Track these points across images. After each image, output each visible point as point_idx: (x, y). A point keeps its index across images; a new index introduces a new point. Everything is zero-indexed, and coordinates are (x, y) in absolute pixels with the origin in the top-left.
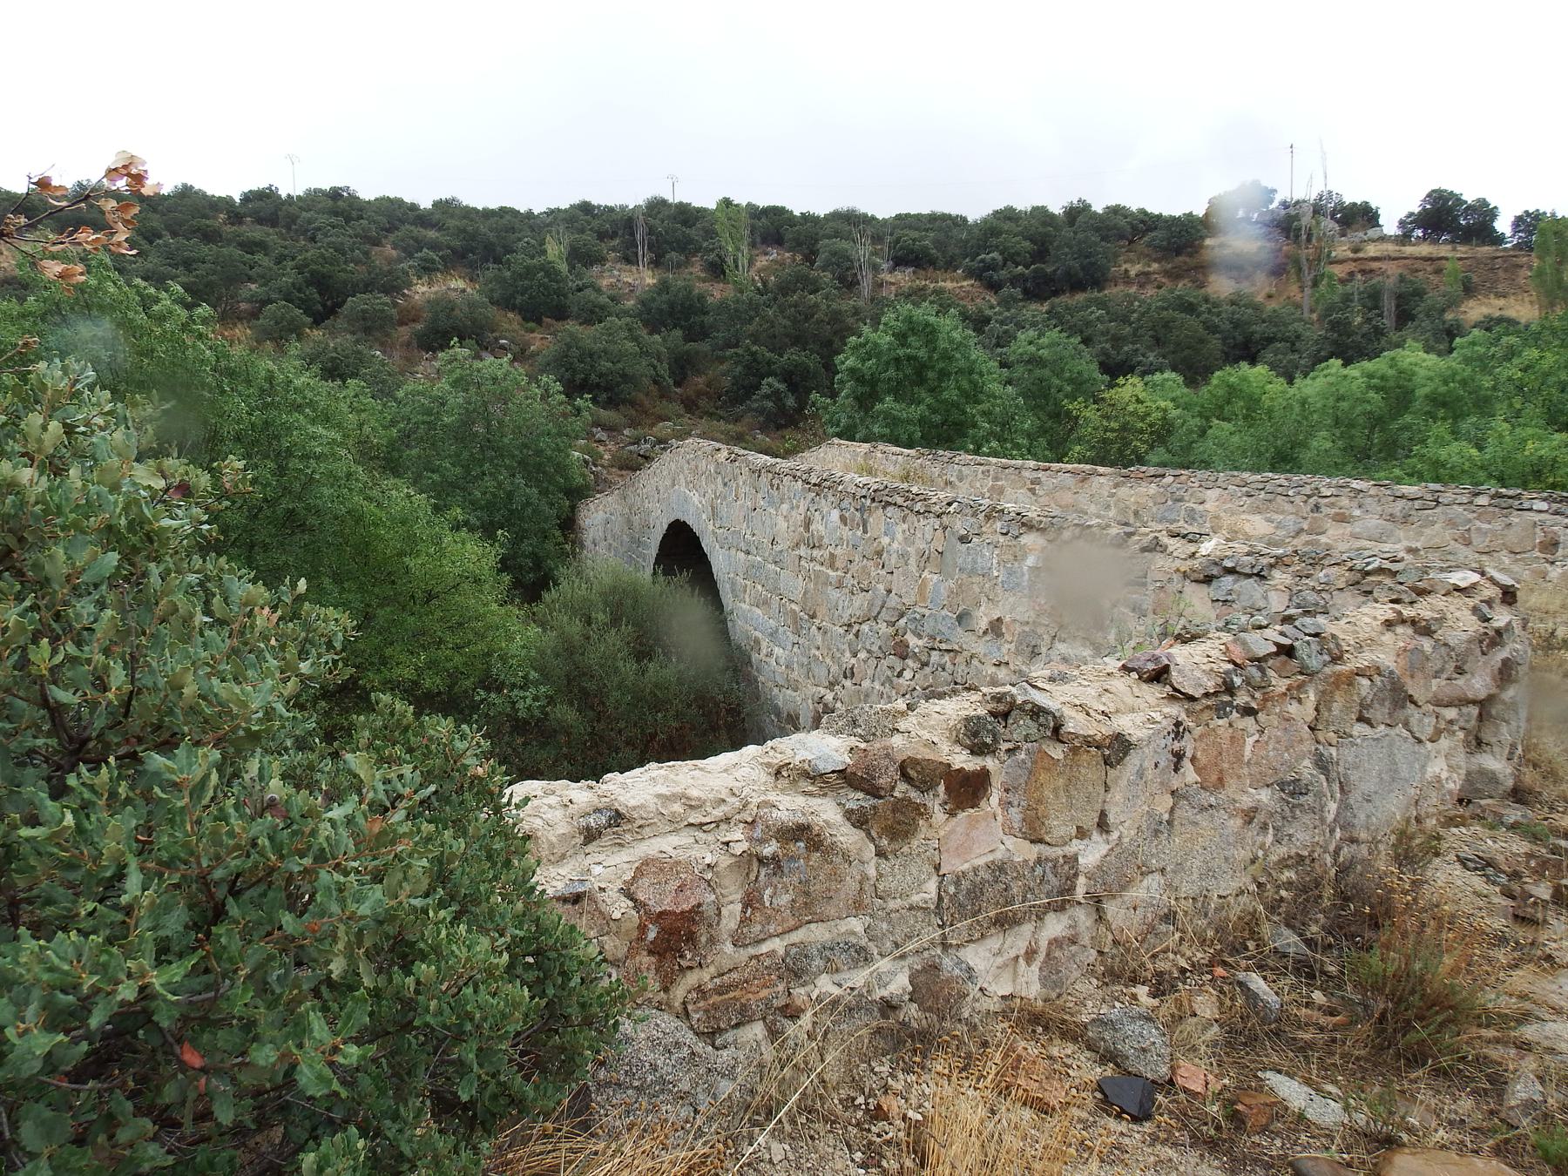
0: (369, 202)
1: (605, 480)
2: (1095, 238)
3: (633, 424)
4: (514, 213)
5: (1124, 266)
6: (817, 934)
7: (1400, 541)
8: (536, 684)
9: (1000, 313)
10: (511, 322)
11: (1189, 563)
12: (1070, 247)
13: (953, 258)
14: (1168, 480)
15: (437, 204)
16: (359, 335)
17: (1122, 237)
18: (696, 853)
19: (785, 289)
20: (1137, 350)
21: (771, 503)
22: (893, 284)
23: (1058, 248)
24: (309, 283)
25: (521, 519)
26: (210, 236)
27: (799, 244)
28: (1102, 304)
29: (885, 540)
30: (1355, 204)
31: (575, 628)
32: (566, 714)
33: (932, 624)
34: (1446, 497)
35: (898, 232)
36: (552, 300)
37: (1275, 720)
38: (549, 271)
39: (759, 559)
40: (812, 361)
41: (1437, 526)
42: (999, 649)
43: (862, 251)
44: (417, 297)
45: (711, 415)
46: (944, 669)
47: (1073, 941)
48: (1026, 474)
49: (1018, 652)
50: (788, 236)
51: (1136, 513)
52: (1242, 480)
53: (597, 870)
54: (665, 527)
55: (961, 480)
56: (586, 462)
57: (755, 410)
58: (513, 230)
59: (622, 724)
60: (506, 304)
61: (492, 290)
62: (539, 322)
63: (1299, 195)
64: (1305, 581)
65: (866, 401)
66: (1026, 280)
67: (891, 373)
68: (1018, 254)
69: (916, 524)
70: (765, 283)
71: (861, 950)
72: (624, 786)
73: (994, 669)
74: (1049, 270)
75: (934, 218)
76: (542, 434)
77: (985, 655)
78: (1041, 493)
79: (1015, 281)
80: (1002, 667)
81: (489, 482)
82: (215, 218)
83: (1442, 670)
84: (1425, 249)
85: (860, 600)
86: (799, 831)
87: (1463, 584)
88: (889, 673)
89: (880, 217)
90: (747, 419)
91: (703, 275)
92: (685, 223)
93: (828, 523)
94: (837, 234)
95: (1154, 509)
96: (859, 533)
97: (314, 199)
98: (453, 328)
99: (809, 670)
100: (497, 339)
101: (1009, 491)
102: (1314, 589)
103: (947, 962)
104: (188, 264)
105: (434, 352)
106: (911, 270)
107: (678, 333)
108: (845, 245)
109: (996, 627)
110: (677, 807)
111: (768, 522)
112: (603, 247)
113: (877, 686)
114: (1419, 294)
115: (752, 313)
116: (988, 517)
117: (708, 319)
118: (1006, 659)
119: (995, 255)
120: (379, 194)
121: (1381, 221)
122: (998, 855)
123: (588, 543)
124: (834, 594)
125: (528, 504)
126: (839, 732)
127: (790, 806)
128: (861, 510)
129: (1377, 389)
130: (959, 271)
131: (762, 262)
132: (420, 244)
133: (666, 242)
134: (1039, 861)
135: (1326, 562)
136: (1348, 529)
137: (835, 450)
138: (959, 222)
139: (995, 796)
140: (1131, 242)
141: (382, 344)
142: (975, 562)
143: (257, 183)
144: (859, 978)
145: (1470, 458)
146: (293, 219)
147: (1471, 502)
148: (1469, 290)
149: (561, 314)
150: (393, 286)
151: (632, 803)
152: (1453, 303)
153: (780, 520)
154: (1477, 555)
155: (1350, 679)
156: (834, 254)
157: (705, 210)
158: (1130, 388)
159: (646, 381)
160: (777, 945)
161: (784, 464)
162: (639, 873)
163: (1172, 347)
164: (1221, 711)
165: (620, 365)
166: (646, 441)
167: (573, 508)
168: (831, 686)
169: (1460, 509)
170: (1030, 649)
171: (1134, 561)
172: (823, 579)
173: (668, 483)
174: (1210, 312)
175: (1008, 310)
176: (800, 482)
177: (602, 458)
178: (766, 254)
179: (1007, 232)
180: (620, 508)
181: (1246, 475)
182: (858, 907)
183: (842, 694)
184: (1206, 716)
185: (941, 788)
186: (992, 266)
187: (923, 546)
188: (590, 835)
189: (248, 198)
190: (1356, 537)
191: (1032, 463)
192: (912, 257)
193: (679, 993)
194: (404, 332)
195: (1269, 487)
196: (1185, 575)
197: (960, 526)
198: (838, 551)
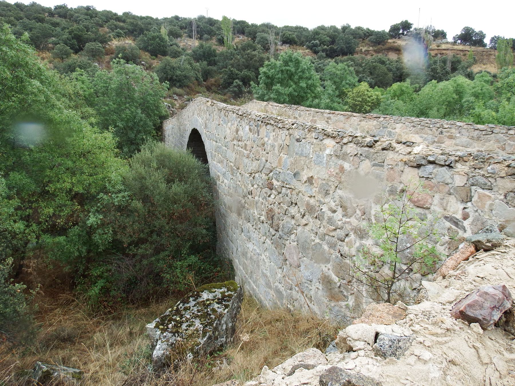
0: (100, 12)
2: (351, 37)
3: (188, 94)
4: (152, 18)
7: (475, 147)
10: (146, 56)
11: (407, 157)
12: (343, 40)
13: (303, 42)
14: (382, 119)
15: (125, 14)
16: (91, 58)
17: (360, 38)
19: (244, 49)
21: (225, 122)
23: (339, 40)
24: (73, 38)
25: (138, 126)
26: (41, 20)
27: (250, 34)
28: (352, 60)
29: (266, 139)
30: (439, 30)
31: (142, 170)
32: (137, 204)
33: (283, 176)
34: (496, 130)
35: (284, 32)
38: (162, 39)
39: (220, 144)
40: (252, 74)
41: (491, 142)
42: (311, 190)
43: (271, 38)
44: (114, 45)
45: (216, 92)
46: (287, 196)
48: (325, 115)
49: (319, 192)
50: (246, 31)
52: (412, 120)
55: (300, 117)
56: (169, 107)
57: (231, 91)
58: (150, 24)
59: (160, 209)
61: (140, 44)
62: (156, 56)
63: (420, 26)
64: (477, 171)
65: (269, 86)
66: (327, 51)
67: (280, 75)
68: (325, 42)
69: (278, 133)
70: (237, 47)
73: (308, 198)
75: (297, 28)
76: (149, 95)
77: (305, 192)
78: (331, 123)
79: (323, 51)
80: (312, 198)
81: (128, 111)
82: (44, 14)
84: (461, 47)
85: (255, 164)
88: (265, 195)
89: (279, 27)
90: (229, 94)
91: (216, 43)
92: (211, 25)
93: (245, 130)
94: (263, 31)
95: (375, 131)
96: (256, 136)
97: (79, 10)
99: (236, 190)
100: (141, 62)
102: (483, 175)
104: (31, 30)
106: (288, 45)
107: (205, 63)
108: (265, 35)
109: (310, 180)
111: (223, 130)
112: (182, 32)
113: (261, 199)
114: (459, 62)
115: (232, 57)
116: (309, 131)
117: (216, 58)
118: (314, 195)
119: (317, 41)
120: (104, 9)
121: (447, 37)
123: (167, 136)
124: (246, 160)
125: (141, 120)
131: (237, 40)
132: (116, 27)
133: (204, 31)
135: (492, 161)
136: (454, 141)
137: (254, 104)
138: (305, 30)
140: (363, 39)
141: (99, 61)
142: (302, 150)
143: (60, 3)
145: (493, 117)
146: (72, 16)
147: (507, 133)
148: (475, 62)
149: (164, 54)
150: (104, 41)
152: (469, 66)
153: (228, 129)
154: (507, 155)
156: (262, 38)
157: (218, 21)
159: (193, 79)
161: (230, 107)
163: (376, 76)
167: (162, 123)
168: (244, 197)
169: (502, 135)
170: (325, 191)
171: (378, 154)
172: (242, 154)
173: (192, 114)
174: (390, 64)
176: (235, 114)
177: (175, 105)
178: (238, 37)
179: (322, 34)
181: (413, 118)
183: (248, 201)
186: (315, 45)
187: (281, 142)
189: (56, 8)
190: (457, 145)
192: (289, 41)
195: (422, 123)
196: (406, 163)
197: (297, 134)
198: (248, 143)
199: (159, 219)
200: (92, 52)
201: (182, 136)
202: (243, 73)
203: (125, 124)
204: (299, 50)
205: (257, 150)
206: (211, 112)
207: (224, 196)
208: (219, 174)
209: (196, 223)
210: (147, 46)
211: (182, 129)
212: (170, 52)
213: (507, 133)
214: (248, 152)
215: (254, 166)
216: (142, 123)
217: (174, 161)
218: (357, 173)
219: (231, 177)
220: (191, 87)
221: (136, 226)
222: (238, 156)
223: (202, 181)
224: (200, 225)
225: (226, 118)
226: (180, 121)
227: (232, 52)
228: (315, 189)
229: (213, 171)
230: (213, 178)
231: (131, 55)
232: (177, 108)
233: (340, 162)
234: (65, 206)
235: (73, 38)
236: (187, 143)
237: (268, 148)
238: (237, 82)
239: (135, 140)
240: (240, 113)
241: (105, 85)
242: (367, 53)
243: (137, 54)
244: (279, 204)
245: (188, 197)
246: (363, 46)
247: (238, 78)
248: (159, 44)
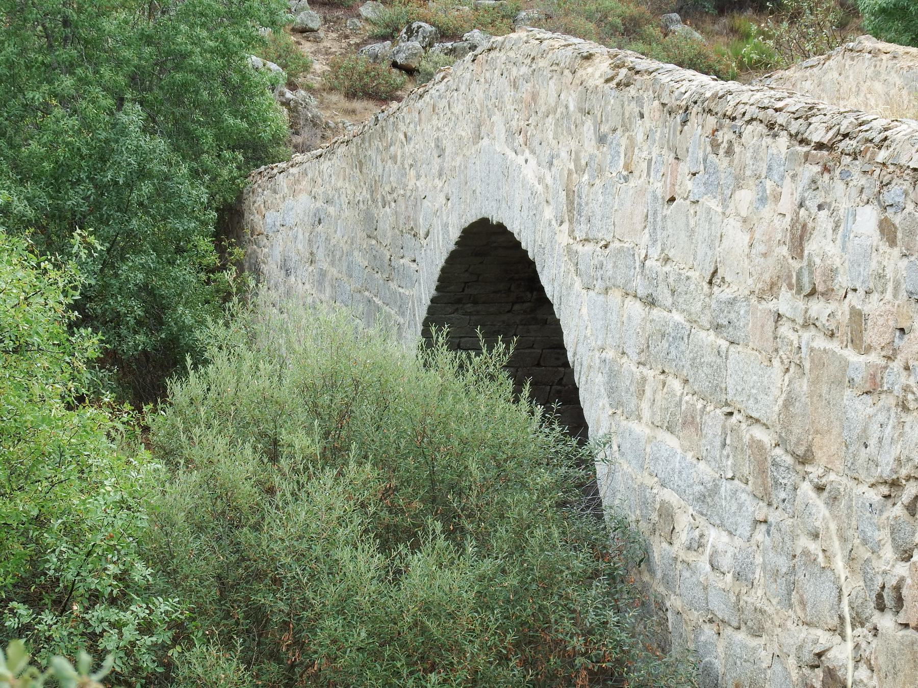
1: (314, 123)
21: (711, 187)
25: (124, 208)
39: (678, 317)
54: (455, 234)
99: (792, 587)
123: (271, 268)
137: (864, 65)
173: (465, 131)
177: (306, 68)
198: (872, 306)
203: (45, 201)
206: (615, 121)
208: (669, 496)
214: (874, 358)
222: (803, 386)
225: (722, 162)
230: (622, 525)
232: (316, 82)
240: (818, 134)
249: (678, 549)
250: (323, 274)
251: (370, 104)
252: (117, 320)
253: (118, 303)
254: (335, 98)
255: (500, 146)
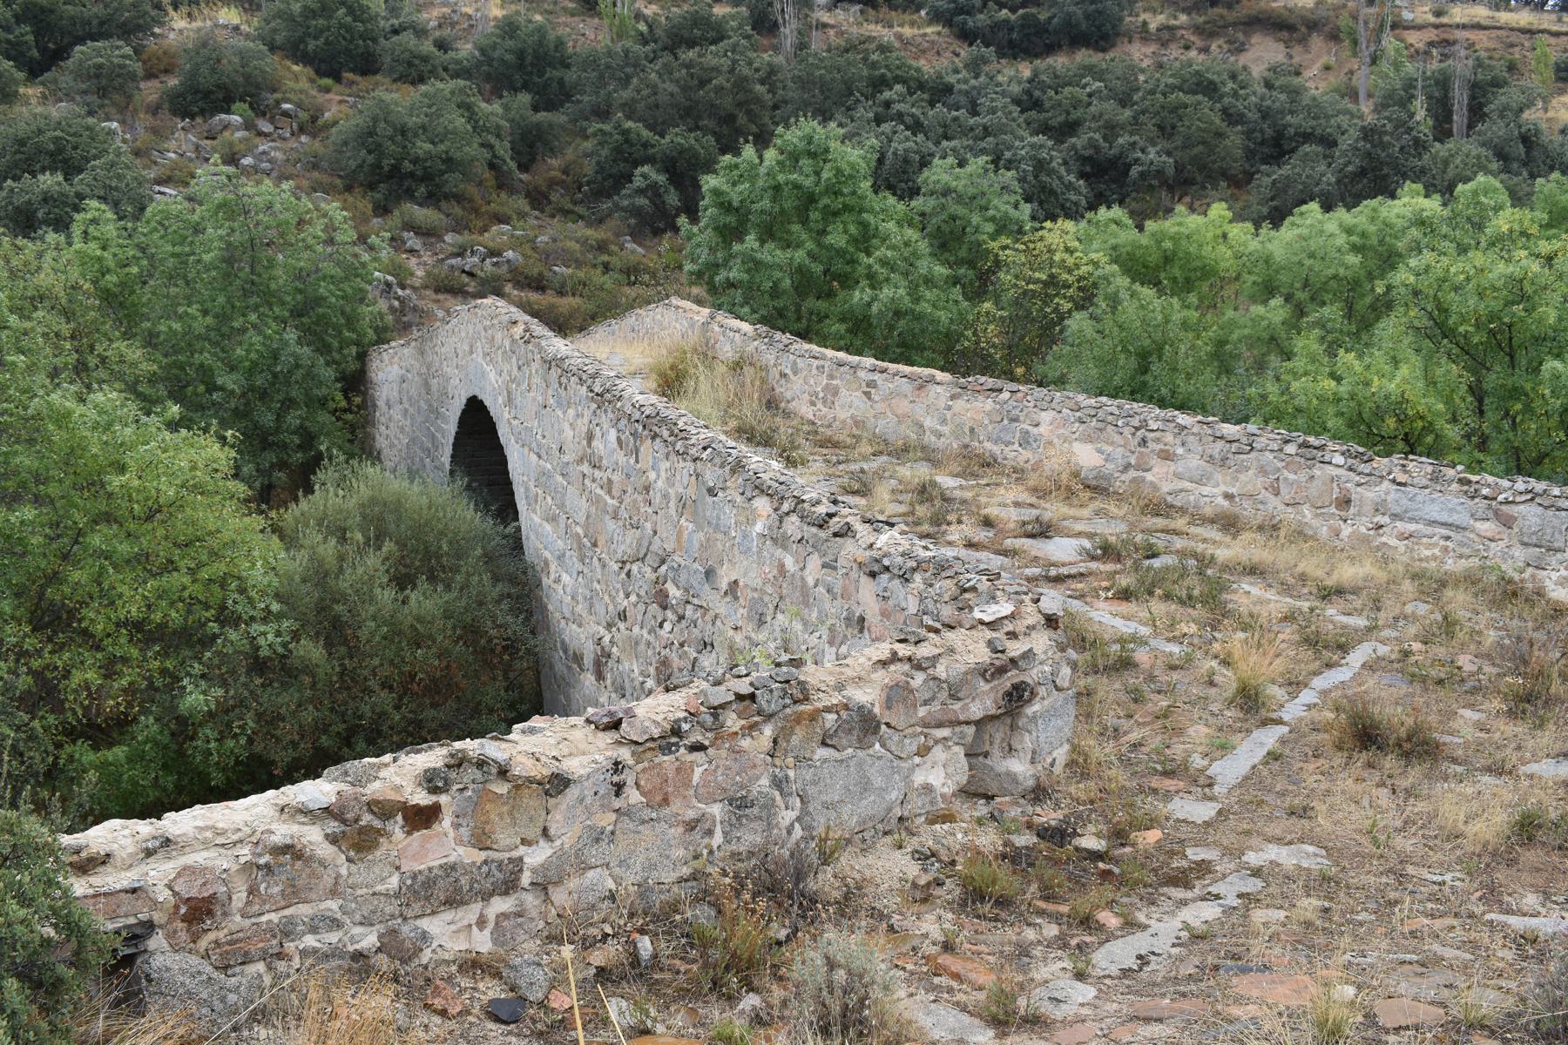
1: (415, 309)
5: (1144, 16)
6: (303, 910)
8: (279, 616)
9: (966, 81)
10: (296, 78)
14: (1006, 395)
18: (218, 862)
20: (1135, 143)
21: (559, 404)
22: (833, 27)
24: (18, 19)
29: (652, 475)
31: (329, 549)
32: (311, 651)
36: (357, 46)
37: (724, 753)
45: (566, 213)
47: (519, 915)
48: (862, 374)
51: (972, 430)
53: (152, 873)
54: (464, 401)
56: (389, 285)
60: (295, 51)
61: (275, 31)
62: (338, 79)
66: (1011, 29)
71: (334, 920)
72: (175, 822)
74: (1042, 17)
76: (324, 278)
78: (877, 398)
83: (933, 699)
86: (288, 850)
87: (987, 619)
90: (615, 222)
93: (607, 442)
96: (632, 461)
98: (218, 86)
100: (278, 103)
101: (843, 392)
103: (405, 929)
105: (193, 119)
106: (858, 7)
107: (525, 98)
110: (209, 834)
115: (629, 70)
117: (571, 76)
122: (452, 859)
123: (381, 403)
124: (611, 525)
126: (335, 780)
127: (283, 832)
128: (634, 434)
129: (1355, 249)
130: (923, 13)
134: (486, 862)
136: (1172, 467)
139: (447, 822)
144: (333, 937)
149: (368, 66)
151: (178, 832)
153: (566, 426)
155: (814, 716)
158: (1060, 234)
160: (274, 917)
162: (179, 875)
164: (667, 749)
165: (442, 147)
166: (473, 252)
167: (362, 357)
173: (467, 348)
174: (1235, 94)
175: (977, 77)
180: (417, 365)
182: (334, 893)
184: (649, 755)
185: (399, 818)
187: (681, 490)
188: (149, 853)
190: (1178, 476)
191: (869, 361)
193: (203, 944)
194: (150, 91)
195: (1101, 414)
197: (711, 476)
198: (616, 478)
199: (371, 692)
200: (97, 76)
201: (435, 413)
202: (668, 138)
204: (901, 25)
205: (635, 501)
207: (563, 622)
208: (547, 554)
209: (479, 703)
210: (302, 40)
211: (434, 388)
212: (387, 60)
213: (1281, 450)
215: (626, 543)
216: (299, 374)
217: (412, 519)
218: (803, 579)
219: (578, 566)
220: (471, 200)
221: (309, 715)
223: (496, 579)
224: (491, 711)
225: (562, 391)
226: (429, 359)
227: (627, 52)
228: (741, 610)
229: (531, 543)
231: (241, 80)
233: (779, 552)
234: (125, 660)
235: (18, 19)
236: (451, 440)
237: (657, 500)
238: (648, 173)
239: (277, 430)
240: (597, 389)
241: (178, 249)
242: (1166, 35)
243: (262, 71)
244: (682, 645)
245: (454, 628)
246: (1155, 12)
247: (650, 160)
248: (349, 29)
249: (550, 582)
250: (406, 411)
251: (448, 296)
252: (285, 446)
253: (285, 437)
254: (428, 292)
255: (480, 360)
